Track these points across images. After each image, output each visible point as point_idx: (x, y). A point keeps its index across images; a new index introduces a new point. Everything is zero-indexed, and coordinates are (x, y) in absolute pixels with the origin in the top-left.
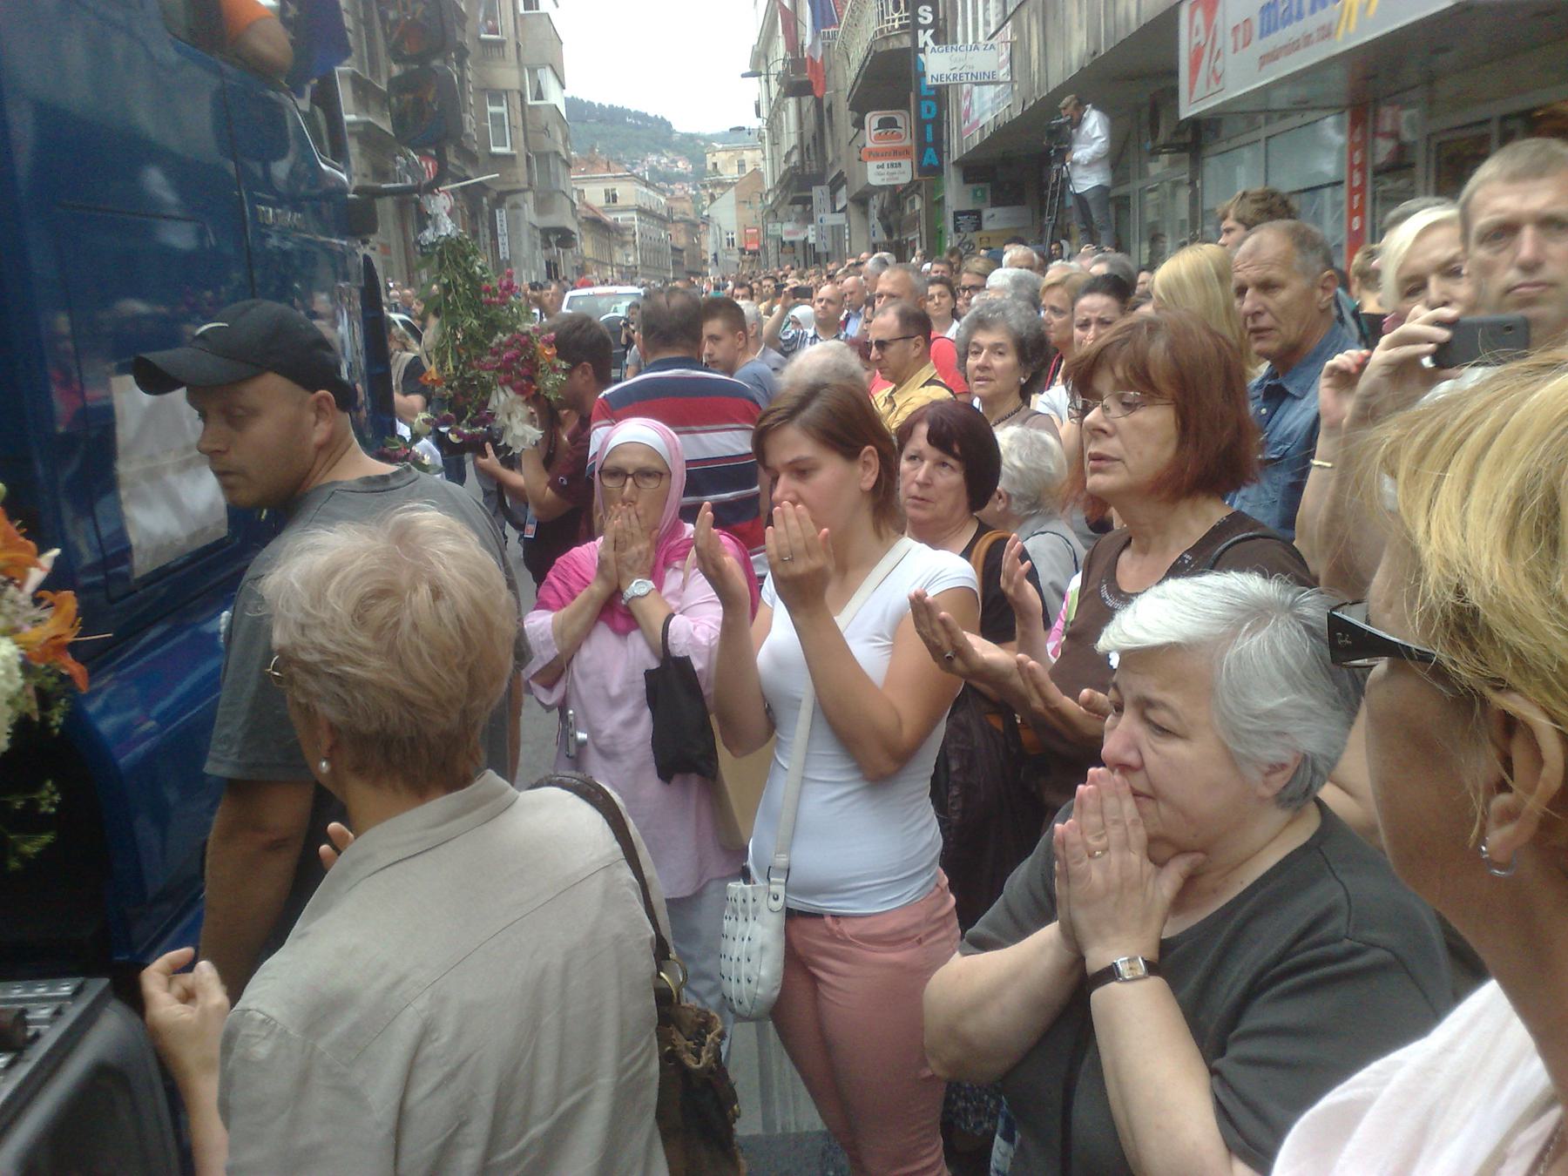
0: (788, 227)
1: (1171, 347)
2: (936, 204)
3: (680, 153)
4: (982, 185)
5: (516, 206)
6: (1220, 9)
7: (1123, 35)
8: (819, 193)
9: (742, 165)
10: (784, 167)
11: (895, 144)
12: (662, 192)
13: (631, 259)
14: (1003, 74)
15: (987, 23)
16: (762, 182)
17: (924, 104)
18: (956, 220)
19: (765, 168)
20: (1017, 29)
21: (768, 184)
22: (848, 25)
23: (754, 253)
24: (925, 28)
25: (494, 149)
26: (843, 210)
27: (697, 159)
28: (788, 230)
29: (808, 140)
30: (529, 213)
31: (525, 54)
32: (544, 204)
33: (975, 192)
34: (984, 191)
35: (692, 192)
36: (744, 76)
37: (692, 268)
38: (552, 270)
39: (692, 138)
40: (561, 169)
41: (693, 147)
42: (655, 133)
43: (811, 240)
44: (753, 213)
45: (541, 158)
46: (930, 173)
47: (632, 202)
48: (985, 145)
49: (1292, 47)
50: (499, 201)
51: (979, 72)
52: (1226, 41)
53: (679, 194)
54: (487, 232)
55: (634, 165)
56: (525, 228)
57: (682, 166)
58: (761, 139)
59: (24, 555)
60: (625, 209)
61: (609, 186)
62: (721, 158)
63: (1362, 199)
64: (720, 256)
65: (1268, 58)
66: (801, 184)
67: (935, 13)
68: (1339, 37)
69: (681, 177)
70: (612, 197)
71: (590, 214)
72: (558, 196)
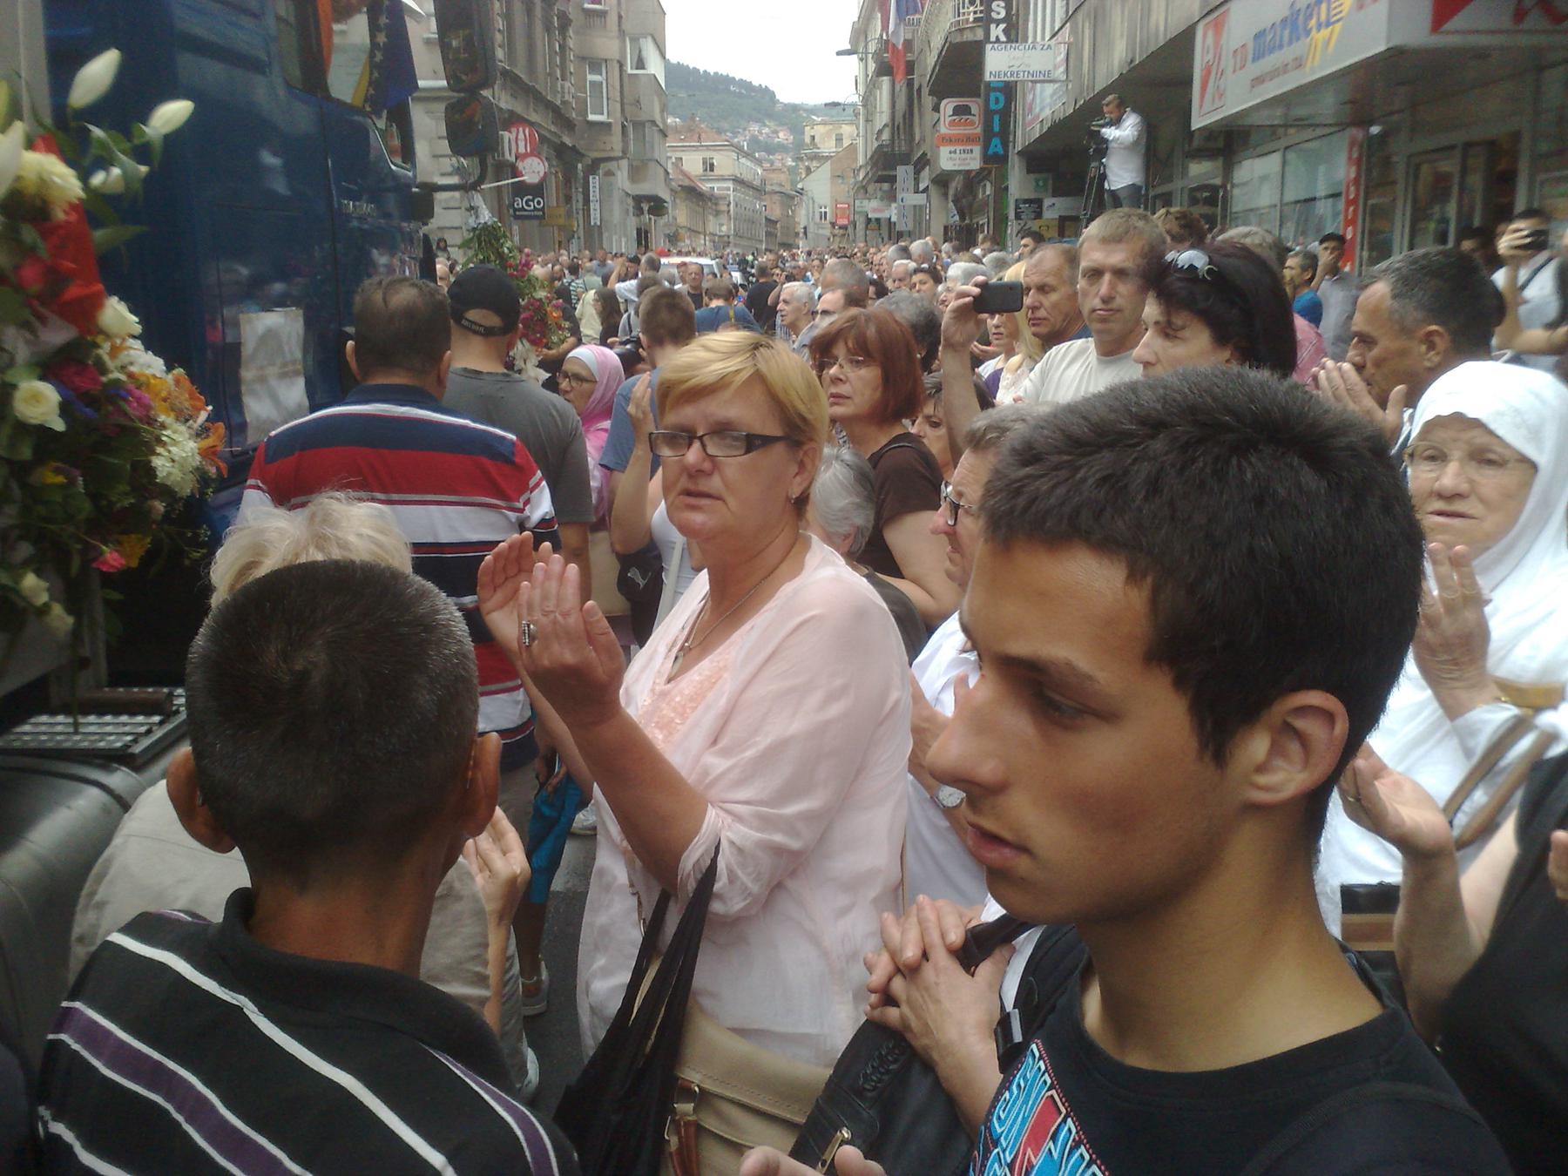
0: (874, 204)
1: (879, 331)
2: (1001, 191)
3: (781, 124)
4: (1044, 175)
5: (610, 173)
6: (1225, 35)
7: (1153, 48)
8: (903, 172)
9: (839, 139)
10: (876, 144)
11: (969, 131)
12: (759, 162)
13: (724, 228)
14: (1060, 73)
15: (1053, 21)
16: (856, 160)
17: (993, 96)
18: (1017, 207)
19: (860, 142)
20: (1074, 32)
21: (861, 161)
22: (930, 13)
23: (844, 227)
24: (998, 22)
25: (591, 117)
26: (926, 190)
27: (797, 130)
28: (872, 207)
29: (899, 119)
30: (622, 179)
31: (627, 26)
32: (637, 171)
33: (1037, 181)
34: (1045, 181)
35: (790, 162)
36: (839, 53)
37: (785, 240)
38: (643, 237)
39: (795, 108)
40: (657, 137)
41: (794, 116)
42: (758, 102)
43: (894, 219)
44: (845, 189)
45: (638, 126)
46: (995, 162)
47: (727, 172)
48: (1042, 138)
49: (1274, 74)
50: (593, 168)
51: (1039, 69)
52: (1228, 63)
53: (778, 164)
54: (580, 197)
55: (735, 134)
56: (617, 195)
57: (783, 136)
58: (857, 115)
59: (198, 404)
60: (722, 179)
61: (708, 154)
62: (819, 131)
63: (1355, 211)
64: (811, 230)
65: (1258, 81)
66: (892, 160)
67: (1008, 8)
68: (1307, 69)
69: (782, 148)
70: (710, 166)
71: (686, 183)
72: (652, 165)
